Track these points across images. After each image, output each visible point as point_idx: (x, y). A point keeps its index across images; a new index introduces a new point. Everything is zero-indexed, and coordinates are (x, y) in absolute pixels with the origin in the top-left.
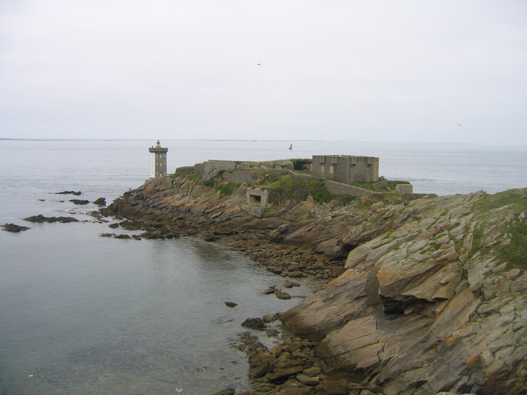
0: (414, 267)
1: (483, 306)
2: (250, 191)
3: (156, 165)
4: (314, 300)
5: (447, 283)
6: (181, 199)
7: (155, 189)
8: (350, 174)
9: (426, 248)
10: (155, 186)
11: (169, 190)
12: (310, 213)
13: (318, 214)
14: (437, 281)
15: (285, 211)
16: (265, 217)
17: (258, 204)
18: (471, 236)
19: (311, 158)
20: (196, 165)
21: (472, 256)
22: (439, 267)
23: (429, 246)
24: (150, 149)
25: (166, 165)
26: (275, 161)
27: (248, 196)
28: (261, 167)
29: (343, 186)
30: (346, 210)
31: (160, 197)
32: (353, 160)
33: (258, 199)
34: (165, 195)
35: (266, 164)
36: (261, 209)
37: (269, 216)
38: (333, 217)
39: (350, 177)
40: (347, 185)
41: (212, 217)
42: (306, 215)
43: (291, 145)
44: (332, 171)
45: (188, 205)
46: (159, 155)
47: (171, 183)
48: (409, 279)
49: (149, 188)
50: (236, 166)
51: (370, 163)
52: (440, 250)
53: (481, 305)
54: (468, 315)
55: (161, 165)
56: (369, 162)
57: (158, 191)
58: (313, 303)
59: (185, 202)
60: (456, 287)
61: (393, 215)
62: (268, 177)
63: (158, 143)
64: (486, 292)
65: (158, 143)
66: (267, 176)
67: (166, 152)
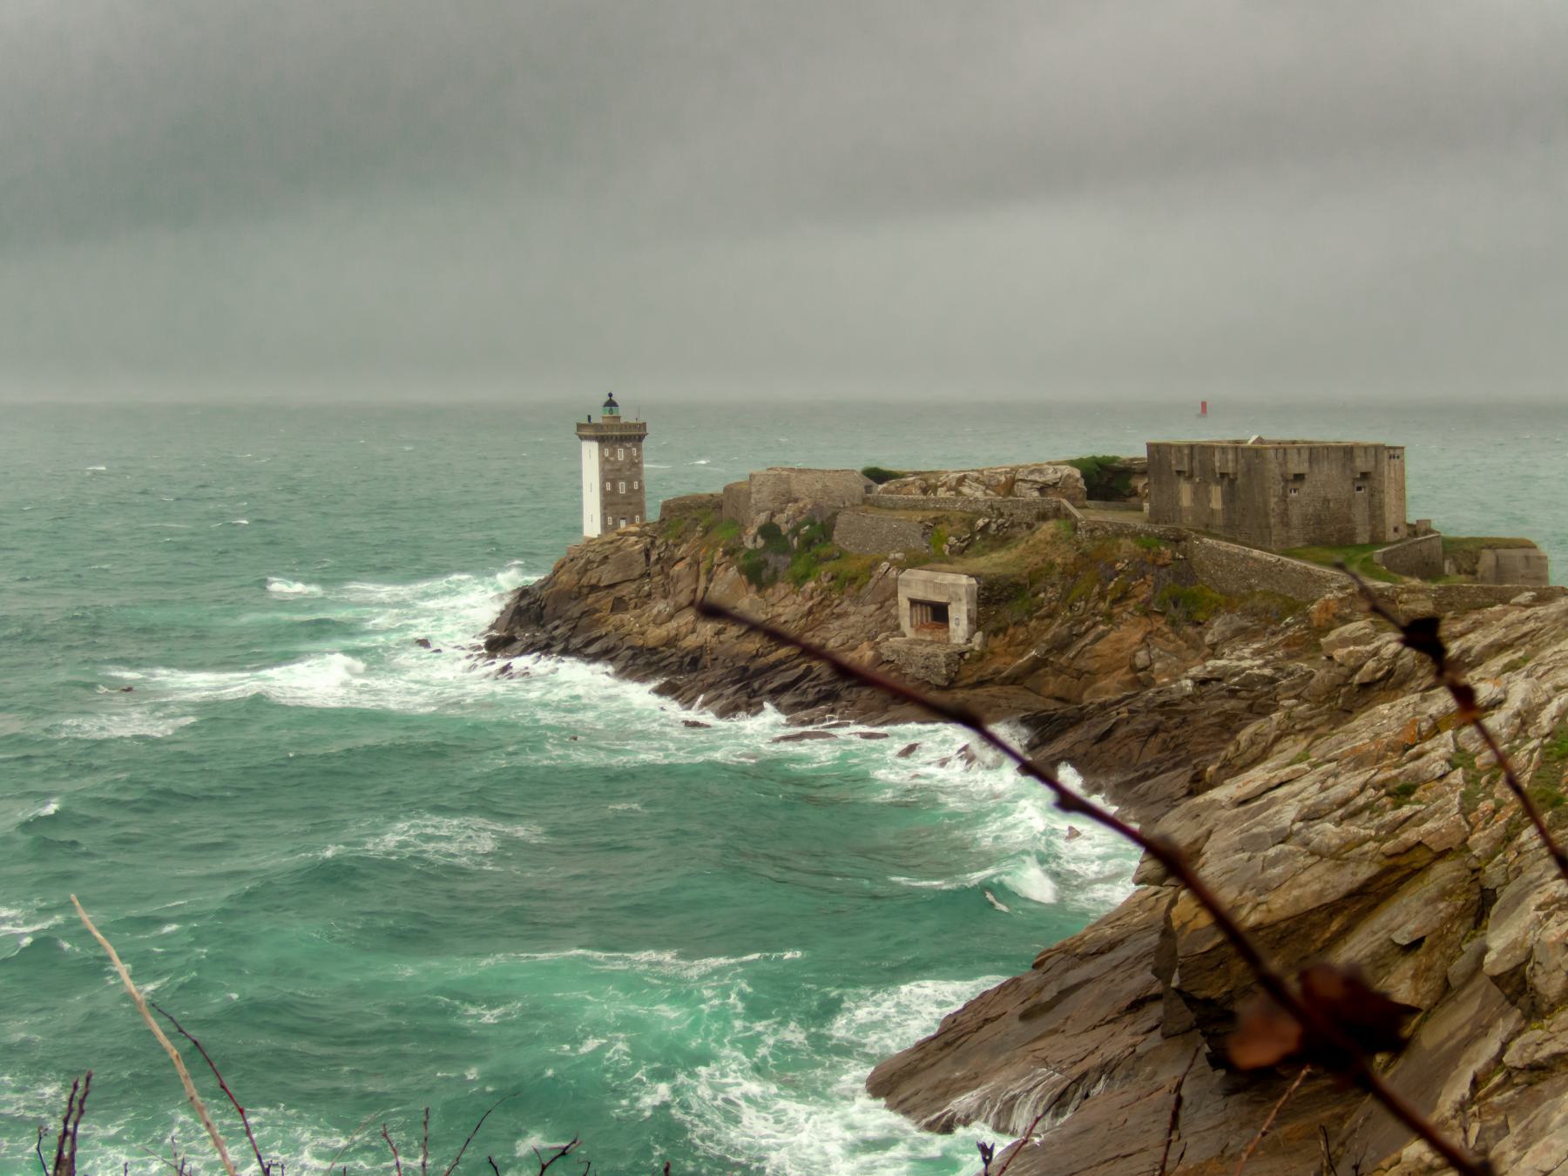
0: (1304, 878)
1: (1525, 1038)
2: (917, 584)
3: (603, 489)
4: (993, 1013)
5: (1416, 944)
6: (671, 617)
7: (584, 581)
8: (1284, 513)
9: (1361, 801)
10: (584, 570)
11: (634, 586)
12: (1134, 668)
13: (1163, 672)
14: (1382, 935)
15: (1038, 663)
16: (966, 686)
17: (940, 634)
18: (1532, 751)
19: (1143, 453)
20: (728, 489)
21: (1519, 834)
22: (1399, 874)
24: (580, 426)
26: (1015, 470)
27: (904, 604)
28: (965, 490)
29: (1255, 560)
31: (597, 611)
33: (939, 613)
34: (619, 605)
36: (948, 656)
37: (981, 683)
38: (1204, 682)
39: (1286, 524)
40: (1273, 558)
41: (770, 687)
42: (1122, 675)
43: (1204, 405)
44: (1216, 503)
45: (691, 642)
46: (613, 453)
47: (642, 558)
48: (1283, 926)
49: (564, 578)
50: (868, 489)
51: (1367, 470)
52: (1406, 810)
53: (1519, 1033)
54: (1469, 1077)
55: (622, 487)
56: (1361, 464)
57: (594, 588)
58: (987, 1021)
59: (684, 630)
60: (1452, 959)
61: (1390, 673)
62: (987, 525)
63: (611, 404)
64: (1540, 981)
65: (611, 404)
66: (981, 523)
67: (640, 438)
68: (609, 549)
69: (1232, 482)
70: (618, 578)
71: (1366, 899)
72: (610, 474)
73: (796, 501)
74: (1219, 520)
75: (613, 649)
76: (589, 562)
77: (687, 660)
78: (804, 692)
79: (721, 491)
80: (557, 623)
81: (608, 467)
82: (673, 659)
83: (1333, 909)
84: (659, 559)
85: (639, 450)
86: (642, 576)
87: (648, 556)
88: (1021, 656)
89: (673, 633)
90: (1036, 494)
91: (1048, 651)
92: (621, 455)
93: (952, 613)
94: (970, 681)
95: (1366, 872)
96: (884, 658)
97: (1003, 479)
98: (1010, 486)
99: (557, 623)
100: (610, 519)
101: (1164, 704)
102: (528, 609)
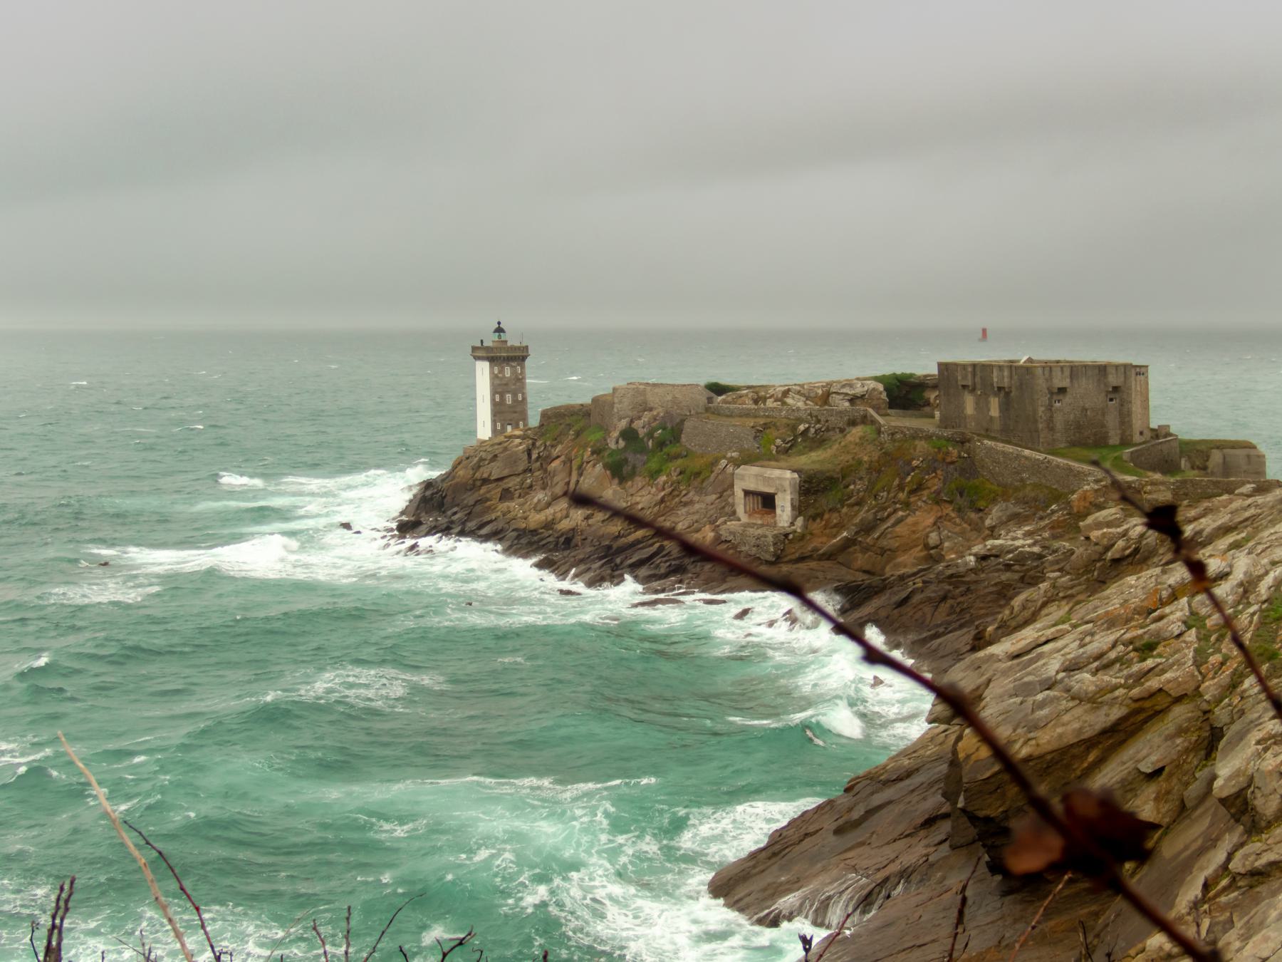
0: (1066, 718)
2: (750, 477)
3: (493, 400)
5: (1158, 772)
6: (549, 505)
7: (478, 475)
9: (1113, 655)
11: (518, 479)
13: (951, 550)
14: (1130, 765)
15: (849, 543)
17: (768, 519)
18: (1253, 614)
21: (1242, 682)
23: (1121, 648)
24: (474, 349)
25: (524, 399)
26: (830, 384)
27: (739, 494)
28: (789, 401)
29: (1026, 458)
30: (1028, 534)
31: (488, 500)
32: (1057, 373)
33: (768, 502)
34: (506, 495)
35: (806, 393)
37: (802, 559)
38: (984, 558)
39: (1051, 429)
41: (630, 562)
42: (918, 552)
44: (995, 412)
45: (565, 525)
46: (501, 371)
47: (525, 457)
48: (1049, 757)
49: (461, 473)
50: (710, 400)
51: (1119, 384)
53: (1242, 845)
54: (1201, 881)
55: (509, 398)
56: (1113, 380)
57: (485, 481)
59: (559, 515)
60: (1187, 784)
61: (1137, 551)
62: (807, 430)
63: (499, 330)
64: (1259, 802)
65: (499, 330)
66: (802, 427)
67: (524, 358)
68: (498, 449)
69: (1008, 394)
70: (506, 472)
71: (1117, 735)
72: (499, 388)
73: (651, 409)
74: (997, 426)
75: (502, 531)
76: (482, 459)
77: (562, 540)
78: (658, 566)
79: (589, 401)
80: (455, 509)
81: (497, 382)
82: (551, 539)
83: (1090, 743)
84: (539, 457)
85: (523, 368)
86: (525, 471)
87: (529, 455)
88: (835, 536)
89: (550, 518)
90: (847, 404)
91: (857, 533)
92: (508, 372)
93: (778, 502)
94: (793, 557)
95: (1116, 713)
96: (723, 538)
97: (820, 392)
98: (826, 398)
99: (455, 509)
100: (499, 424)
101: (951, 576)
102: (431, 499)
